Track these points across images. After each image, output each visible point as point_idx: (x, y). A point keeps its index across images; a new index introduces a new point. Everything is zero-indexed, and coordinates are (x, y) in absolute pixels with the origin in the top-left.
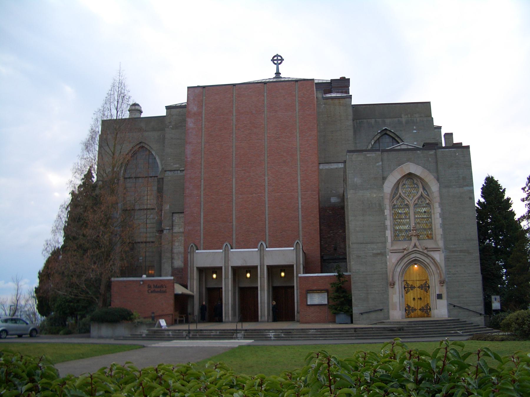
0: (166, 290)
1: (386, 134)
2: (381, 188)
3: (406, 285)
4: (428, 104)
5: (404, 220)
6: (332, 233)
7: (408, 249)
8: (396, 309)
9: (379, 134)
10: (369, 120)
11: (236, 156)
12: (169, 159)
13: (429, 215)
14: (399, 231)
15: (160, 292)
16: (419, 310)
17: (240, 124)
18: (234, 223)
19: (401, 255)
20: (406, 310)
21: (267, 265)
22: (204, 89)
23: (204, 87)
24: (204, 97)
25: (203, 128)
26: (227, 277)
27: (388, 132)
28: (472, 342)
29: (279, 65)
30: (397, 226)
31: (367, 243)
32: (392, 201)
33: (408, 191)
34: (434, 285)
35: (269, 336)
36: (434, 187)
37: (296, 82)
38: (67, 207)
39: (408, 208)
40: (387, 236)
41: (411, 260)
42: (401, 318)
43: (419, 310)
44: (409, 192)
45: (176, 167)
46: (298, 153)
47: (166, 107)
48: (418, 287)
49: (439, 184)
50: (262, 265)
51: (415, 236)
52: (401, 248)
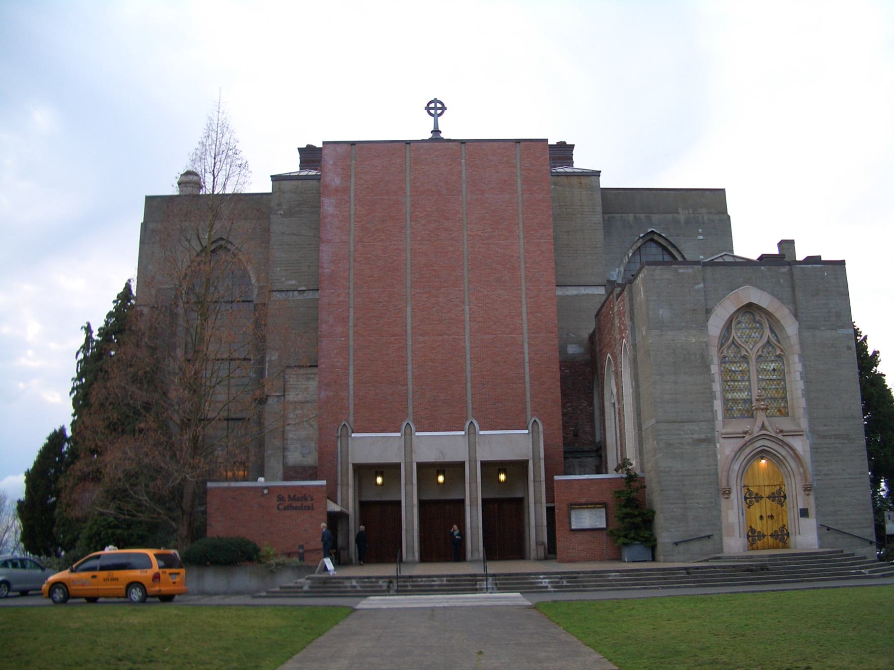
0: (312, 504)
1: (652, 240)
2: (703, 327)
3: (747, 494)
4: (722, 192)
5: (740, 383)
6: (569, 407)
7: (752, 433)
8: (734, 536)
9: (641, 240)
10: (623, 215)
11: (412, 267)
12: (278, 269)
13: (781, 375)
14: (732, 402)
15: (302, 509)
16: (770, 536)
17: (418, 211)
18: (410, 386)
19: (741, 442)
20: (748, 536)
21: (481, 461)
22: (353, 146)
23: (353, 143)
24: (354, 162)
25: (352, 216)
26: (409, 482)
27: (656, 238)
28: (83, 585)
29: (439, 118)
30: (730, 393)
31: (682, 422)
32: (721, 350)
33: (746, 334)
34: (794, 494)
35: (541, 585)
36: (791, 328)
37: (516, 142)
38: (78, 353)
39: (746, 362)
40: (716, 410)
41: (758, 450)
42: (742, 551)
43: (770, 536)
44: (748, 335)
45: (291, 285)
46: (523, 266)
47: (271, 176)
48: (767, 497)
49: (799, 324)
50: (473, 460)
51: (762, 409)
52: (740, 430)
